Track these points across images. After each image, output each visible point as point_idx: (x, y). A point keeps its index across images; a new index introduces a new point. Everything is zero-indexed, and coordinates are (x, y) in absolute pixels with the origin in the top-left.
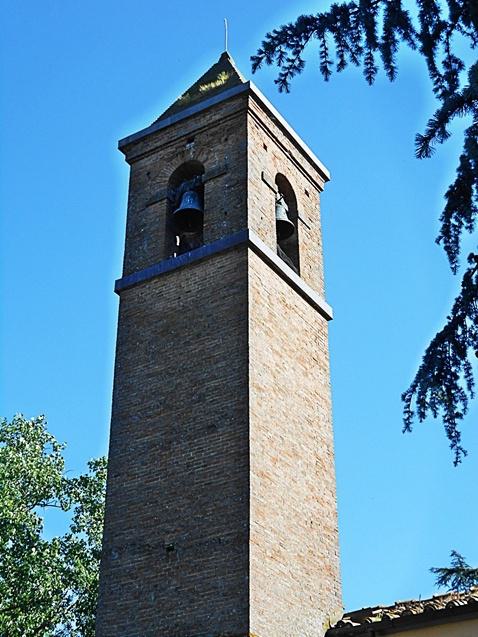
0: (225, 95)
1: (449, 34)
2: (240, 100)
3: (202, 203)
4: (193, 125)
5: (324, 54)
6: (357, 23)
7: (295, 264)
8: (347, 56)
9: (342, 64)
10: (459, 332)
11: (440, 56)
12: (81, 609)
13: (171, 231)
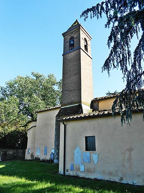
0: (77, 26)
1: (110, 11)
2: (79, 27)
3: (74, 43)
4: (72, 31)
5: (91, 15)
6: (96, 9)
7: (87, 51)
8: (94, 15)
9: (94, 16)
10: (110, 58)
11: (109, 14)
12: (59, 99)
13: (70, 47)
